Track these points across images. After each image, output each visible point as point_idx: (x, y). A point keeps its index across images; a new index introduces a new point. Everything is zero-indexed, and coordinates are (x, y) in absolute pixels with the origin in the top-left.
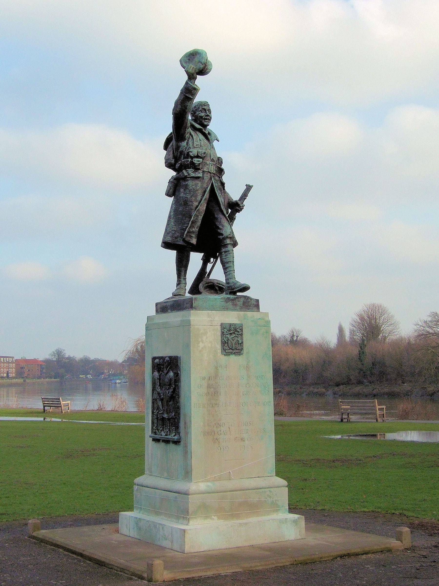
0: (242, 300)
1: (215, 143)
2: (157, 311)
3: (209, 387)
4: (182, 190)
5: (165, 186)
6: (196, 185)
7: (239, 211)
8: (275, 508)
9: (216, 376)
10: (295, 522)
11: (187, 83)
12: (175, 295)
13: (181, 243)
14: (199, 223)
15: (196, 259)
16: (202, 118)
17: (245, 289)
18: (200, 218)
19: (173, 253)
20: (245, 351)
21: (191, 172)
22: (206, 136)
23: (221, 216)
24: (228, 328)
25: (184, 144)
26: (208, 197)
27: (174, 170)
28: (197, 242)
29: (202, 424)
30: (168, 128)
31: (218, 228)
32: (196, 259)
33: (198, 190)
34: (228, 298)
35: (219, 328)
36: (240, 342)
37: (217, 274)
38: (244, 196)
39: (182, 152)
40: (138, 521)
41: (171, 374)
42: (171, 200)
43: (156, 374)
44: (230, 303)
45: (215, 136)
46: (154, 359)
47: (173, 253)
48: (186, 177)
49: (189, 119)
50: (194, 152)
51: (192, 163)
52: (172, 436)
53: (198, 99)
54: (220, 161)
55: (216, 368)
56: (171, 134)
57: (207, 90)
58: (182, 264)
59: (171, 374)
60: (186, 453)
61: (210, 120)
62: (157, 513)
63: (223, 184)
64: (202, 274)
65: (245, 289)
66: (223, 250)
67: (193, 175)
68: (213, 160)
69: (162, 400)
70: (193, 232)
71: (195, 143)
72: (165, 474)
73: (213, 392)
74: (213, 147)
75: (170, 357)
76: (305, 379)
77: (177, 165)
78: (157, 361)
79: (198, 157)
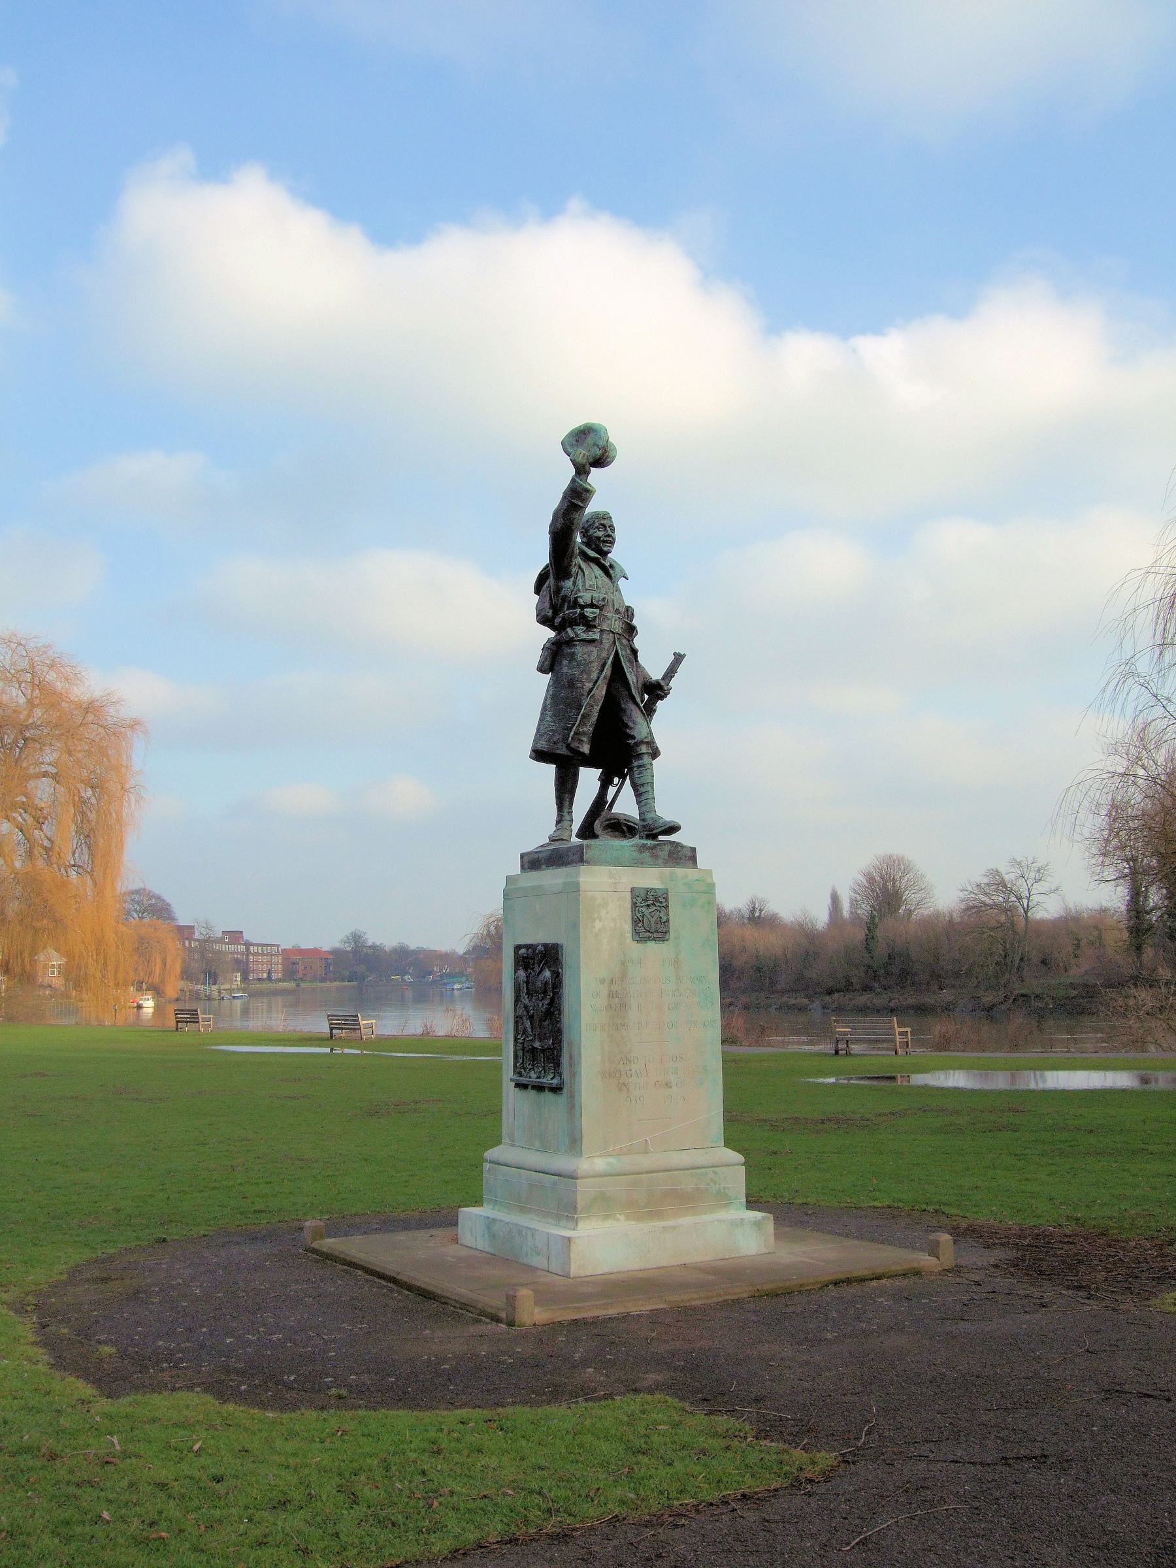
0: (667, 848)
1: (621, 583)
2: (522, 867)
3: (611, 995)
4: (565, 662)
5: (536, 655)
6: (590, 653)
7: (661, 698)
8: (723, 1200)
9: (624, 976)
10: (757, 1224)
11: (573, 480)
12: (553, 840)
13: (563, 751)
14: (594, 718)
15: (589, 779)
16: (600, 541)
17: (672, 829)
18: (597, 709)
19: (551, 769)
20: (672, 935)
21: (580, 632)
22: (607, 570)
23: (632, 706)
24: (643, 896)
25: (568, 584)
26: (609, 673)
27: (553, 627)
28: (591, 750)
29: (599, 1058)
30: (541, 557)
31: (627, 726)
32: (589, 779)
33: (592, 661)
34: (644, 846)
35: (628, 896)
36: (664, 919)
37: (625, 804)
38: (671, 673)
39: (565, 598)
40: (490, 1223)
41: (547, 974)
42: (548, 677)
43: (522, 974)
44: (647, 854)
45: (622, 570)
46: (518, 948)
47: (551, 769)
48: (572, 640)
49: (577, 542)
50: (585, 598)
51: (583, 616)
52: (548, 1080)
53: (593, 507)
54: (629, 612)
55: (623, 963)
56: (547, 566)
57: (606, 492)
58: (565, 788)
59: (547, 974)
60: (573, 1108)
61: (612, 543)
62: (523, 1210)
63: (635, 652)
64: (600, 804)
65: (672, 829)
66: (636, 764)
67: (584, 636)
68: (617, 611)
69: (531, 1018)
70: (584, 733)
71: (587, 583)
72: (537, 1144)
73: (617, 1004)
74: (618, 590)
75: (545, 945)
76: (779, 985)
77: (558, 620)
78: (523, 951)
79: (592, 605)
